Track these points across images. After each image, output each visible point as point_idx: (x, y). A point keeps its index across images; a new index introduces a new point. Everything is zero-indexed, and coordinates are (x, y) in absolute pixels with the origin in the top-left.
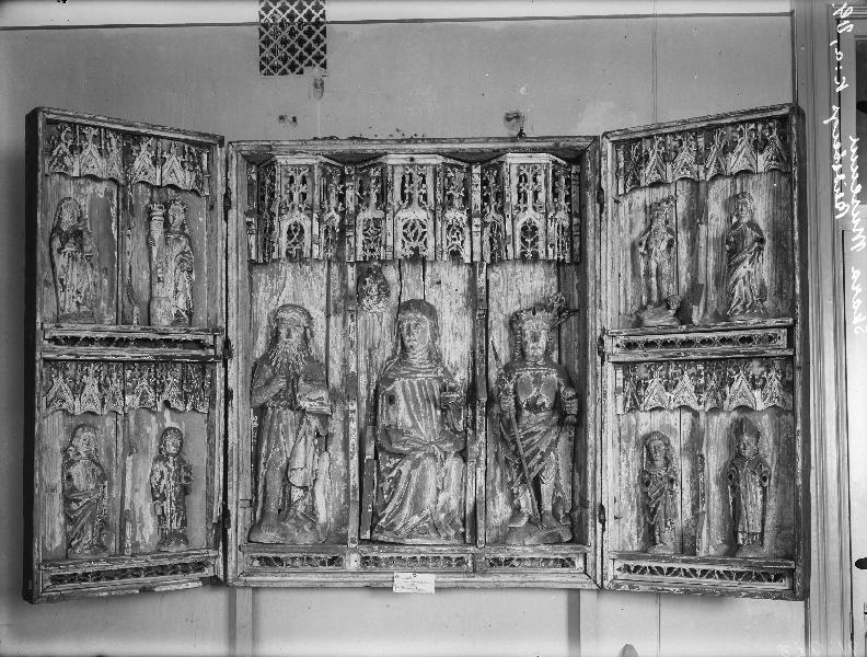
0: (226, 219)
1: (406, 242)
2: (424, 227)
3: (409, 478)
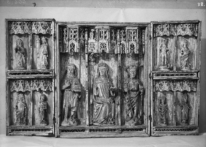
1: (101, 48)
2: (106, 45)
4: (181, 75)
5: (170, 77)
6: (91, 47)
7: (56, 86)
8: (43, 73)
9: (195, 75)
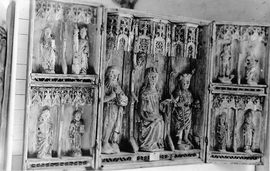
0: (101, 34)
1: (157, 48)
2: (162, 44)
3: (154, 129)
4: (246, 90)
5: (232, 92)
6: (141, 46)
7: (100, 96)
8: (82, 80)
9: (263, 90)
